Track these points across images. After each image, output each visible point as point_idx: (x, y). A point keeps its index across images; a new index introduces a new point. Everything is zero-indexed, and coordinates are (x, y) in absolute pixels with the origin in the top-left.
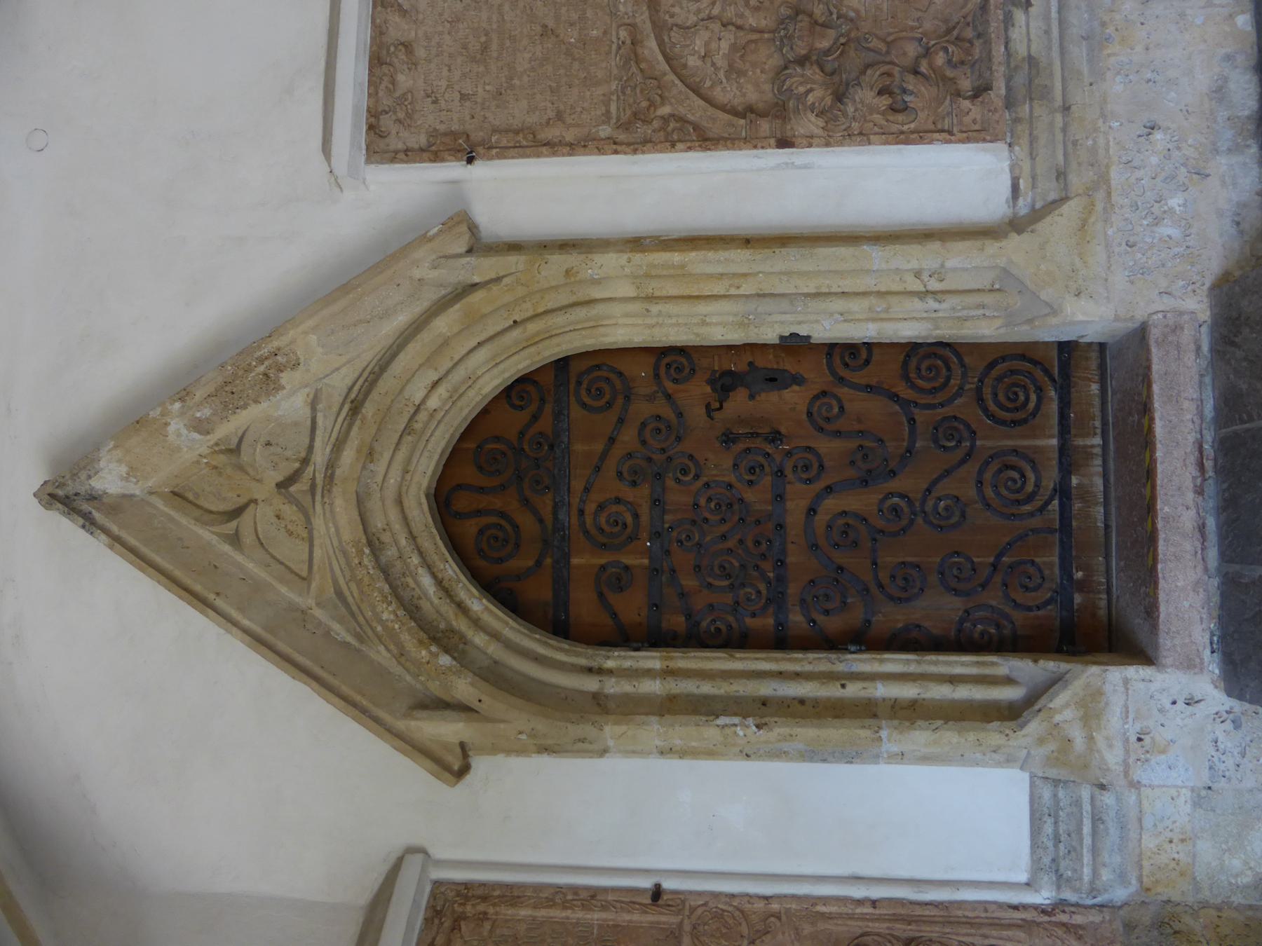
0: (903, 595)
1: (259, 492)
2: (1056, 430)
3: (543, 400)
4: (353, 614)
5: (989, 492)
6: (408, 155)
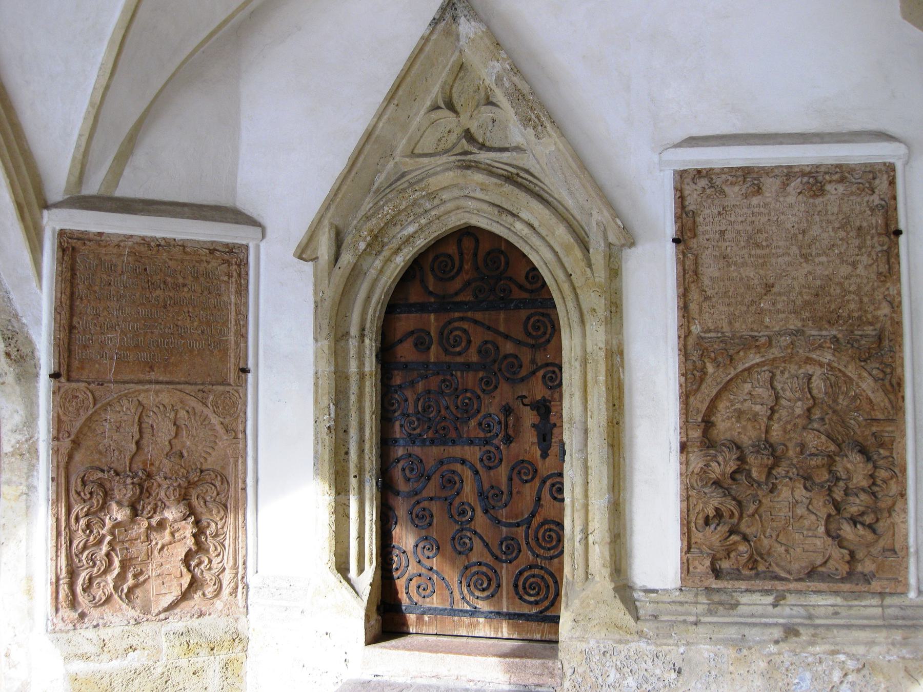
0: (414, 515)
1: (464, 118)
2: (511, 611)
3: (531, 291)
4: (391, 185)
5: (475, 569)
6: (681, 198)
